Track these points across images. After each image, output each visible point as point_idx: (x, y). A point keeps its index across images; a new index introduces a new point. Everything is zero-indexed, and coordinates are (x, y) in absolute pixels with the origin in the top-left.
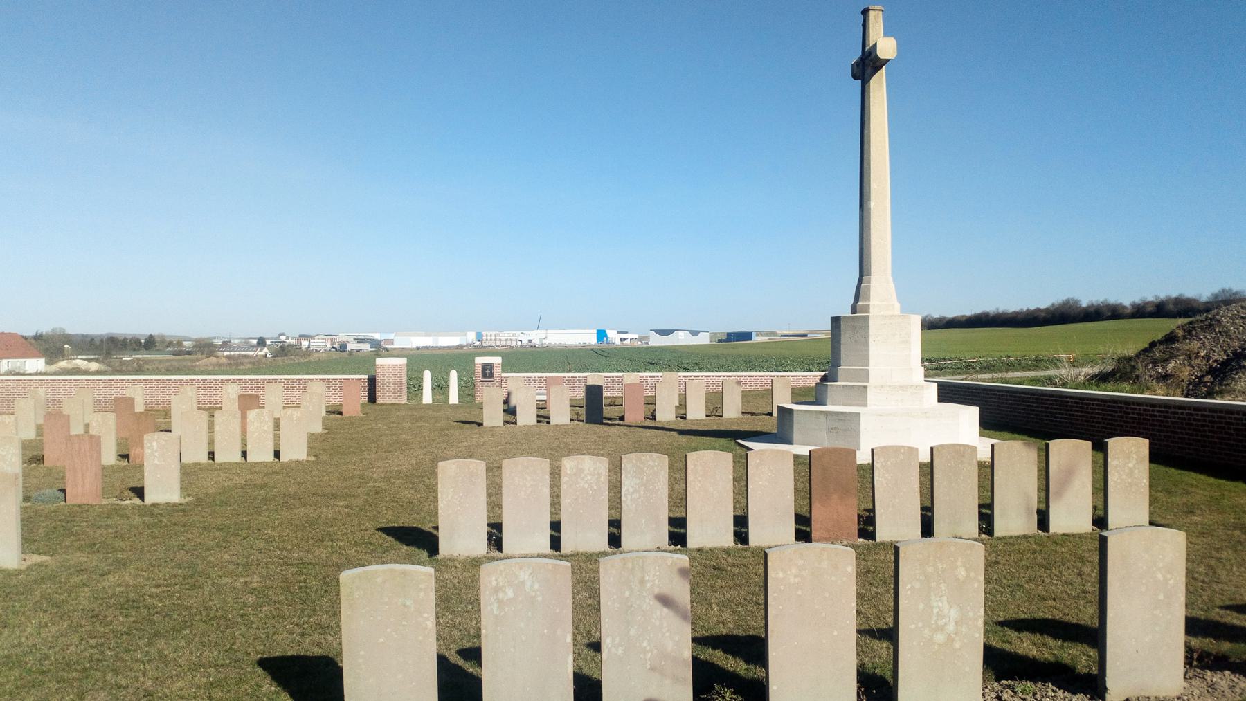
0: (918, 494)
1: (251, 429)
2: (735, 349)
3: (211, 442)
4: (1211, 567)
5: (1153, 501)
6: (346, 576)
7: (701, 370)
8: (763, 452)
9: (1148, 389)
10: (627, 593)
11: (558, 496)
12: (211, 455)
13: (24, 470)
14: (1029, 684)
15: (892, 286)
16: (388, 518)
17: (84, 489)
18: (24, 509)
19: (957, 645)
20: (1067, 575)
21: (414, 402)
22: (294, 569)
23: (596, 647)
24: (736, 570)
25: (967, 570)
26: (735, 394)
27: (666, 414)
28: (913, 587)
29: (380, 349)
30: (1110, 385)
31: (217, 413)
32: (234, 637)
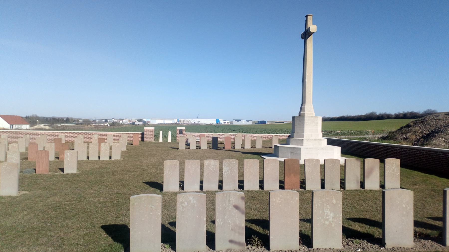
0: (320, 175)
1: (102, 149)
2: (261, 126)
3: (88, 153)
4: (423, 204)
5: (401, 180)
6: (132, 198)
7: (249, 133)
8: (269, 160)
9: (400, 142)
10: (224, 205)
11: (203, 172)
12: (88, 158)
13: (20, 162)
14: (358, 240)
15: (313, 107)
16: (147, 179)
17: (42, 168)
18: (20, 176)
19: (333, 226)
20: (371, 204)
21: (156, 141)
22: (115, 196)
23: (214, 222)
24: (260, 198)
25: (336, 200)
26: (260, 140)
27: (238, 147)
28: (318, 206)
29: (146, 124)
30: (386, 141)
31: (90, 144)
32: (93, 218)
